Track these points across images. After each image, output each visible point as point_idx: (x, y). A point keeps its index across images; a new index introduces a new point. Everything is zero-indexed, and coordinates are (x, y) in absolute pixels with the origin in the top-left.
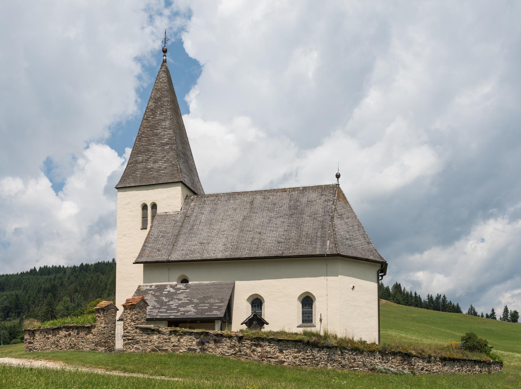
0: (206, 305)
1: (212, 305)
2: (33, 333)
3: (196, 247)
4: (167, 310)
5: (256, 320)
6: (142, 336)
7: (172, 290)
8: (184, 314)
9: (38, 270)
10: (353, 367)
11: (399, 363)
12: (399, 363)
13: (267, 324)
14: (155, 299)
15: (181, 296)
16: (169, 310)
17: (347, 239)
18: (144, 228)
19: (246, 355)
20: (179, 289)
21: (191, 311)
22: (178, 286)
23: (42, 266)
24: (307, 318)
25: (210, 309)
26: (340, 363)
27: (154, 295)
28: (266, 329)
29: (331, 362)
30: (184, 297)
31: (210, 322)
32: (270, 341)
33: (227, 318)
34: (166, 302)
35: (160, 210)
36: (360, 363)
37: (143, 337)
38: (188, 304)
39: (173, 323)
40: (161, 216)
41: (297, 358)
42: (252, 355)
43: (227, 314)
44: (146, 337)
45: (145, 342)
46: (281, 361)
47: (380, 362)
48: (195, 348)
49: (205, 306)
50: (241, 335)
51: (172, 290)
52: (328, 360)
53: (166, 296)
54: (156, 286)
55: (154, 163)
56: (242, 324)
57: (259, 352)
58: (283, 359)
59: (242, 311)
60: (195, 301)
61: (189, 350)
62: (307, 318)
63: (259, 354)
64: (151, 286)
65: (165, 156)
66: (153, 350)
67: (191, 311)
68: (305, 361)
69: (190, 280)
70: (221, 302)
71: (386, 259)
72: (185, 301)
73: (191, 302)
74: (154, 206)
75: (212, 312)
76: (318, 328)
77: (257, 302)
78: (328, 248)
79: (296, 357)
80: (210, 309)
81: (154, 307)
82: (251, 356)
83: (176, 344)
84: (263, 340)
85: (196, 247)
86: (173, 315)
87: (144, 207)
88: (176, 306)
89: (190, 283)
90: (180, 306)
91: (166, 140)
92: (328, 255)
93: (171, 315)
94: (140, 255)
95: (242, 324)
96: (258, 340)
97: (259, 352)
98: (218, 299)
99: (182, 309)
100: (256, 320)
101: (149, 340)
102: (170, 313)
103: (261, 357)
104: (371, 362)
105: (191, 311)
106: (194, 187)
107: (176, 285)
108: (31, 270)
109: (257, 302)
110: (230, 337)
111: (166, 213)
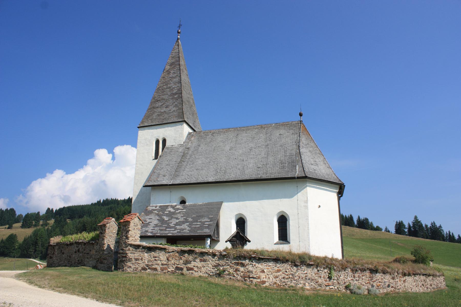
0: (199, 223)
1: (203, 223)
2: (53, 248)
3: (192, 173)
4: (167, 228)
5: (240, 238)
6: (134, 253)
7: (172, 210)
8: (180, 232)
9: (102, 202)
10: (329, 286)
11: (368, 280)
12: (368, 280)
13: (249, 241)
14: (158, 218)
15: (179, 216)
16: (168, 228)
17: (312, 164)
18: (156, 157)
19: (229, 274)
20: (178, 209)
21: (185, 229)
22: (177, 207)
23: (105, 199)
24: (283, 236)
25: (201, 228)
26: (317, 282)
27: (158, 215)
28: (248, 247)
29: (309, 281)
30: (182, 216)
31: (201, 239)
32: (251, 258)
33: (216, 236)
34: (167, 221)
35: (168, 144)
36: (335, 281)
37: (135, 255)
38: (183, 223)
39: (172, 240)
40: (168, 148)
41: (278, 277)
42: (235, 275)
43: (216, 232)
44: (138, 255)
45: (136, 259)
46: (263, 281)
47: (352, 280)
48: (182, 266)
49: (198, 225)
50: (225, 253)
51: (172, 210)
52: (306, 279)
53: (167, 215)
54: (160, 206)
55: (166, 107)
56: (226, 242)
57: (242, 272)
58: (264, 280)
59: (228, 228)
60: (190, 220)
61: (177, 268)
62: (283, 236)
63: (242, 274)
64: (156, 207)
65: (174, 103)
66: (144, 269)
67: (186, 230)
68: (286, 281)
69: (187, 201)
70: (210, 221)
71: (344, 181)
72: (182, 219)
73: (186, 221)
74: (164, 141)
75: (203, 230)
76: (295, 246)
77: (241, 223)
78: (298, 172)
79: (276, 277)
80: (201, 228)
81: (156, 226)
82: (234, 276)
83: (165, 263)
84: (245, 258)
85: (192, 173)
86: (171, 233)
87: (157, 142)
88: (174, 224)
89: (187, 204)
90: (177, 224)
91: (175, 92)
92: (298, 178)
93: (169, 233)
94: (148, 180)
95: (226, 242)
96: (242, 258)
97: (242, 272)
98: (209, 218)
99: (178, 227)
100: (240, 238)
101: (140, 258)
102: (169, 231)
103: (244, 277)
104: (344, 280)
105: (185, 229)
106: (195, 126)
107: (176, 205)
108: (98, 202)
109: (241, 223)
110: (214, 255)
111: (172, 146)
